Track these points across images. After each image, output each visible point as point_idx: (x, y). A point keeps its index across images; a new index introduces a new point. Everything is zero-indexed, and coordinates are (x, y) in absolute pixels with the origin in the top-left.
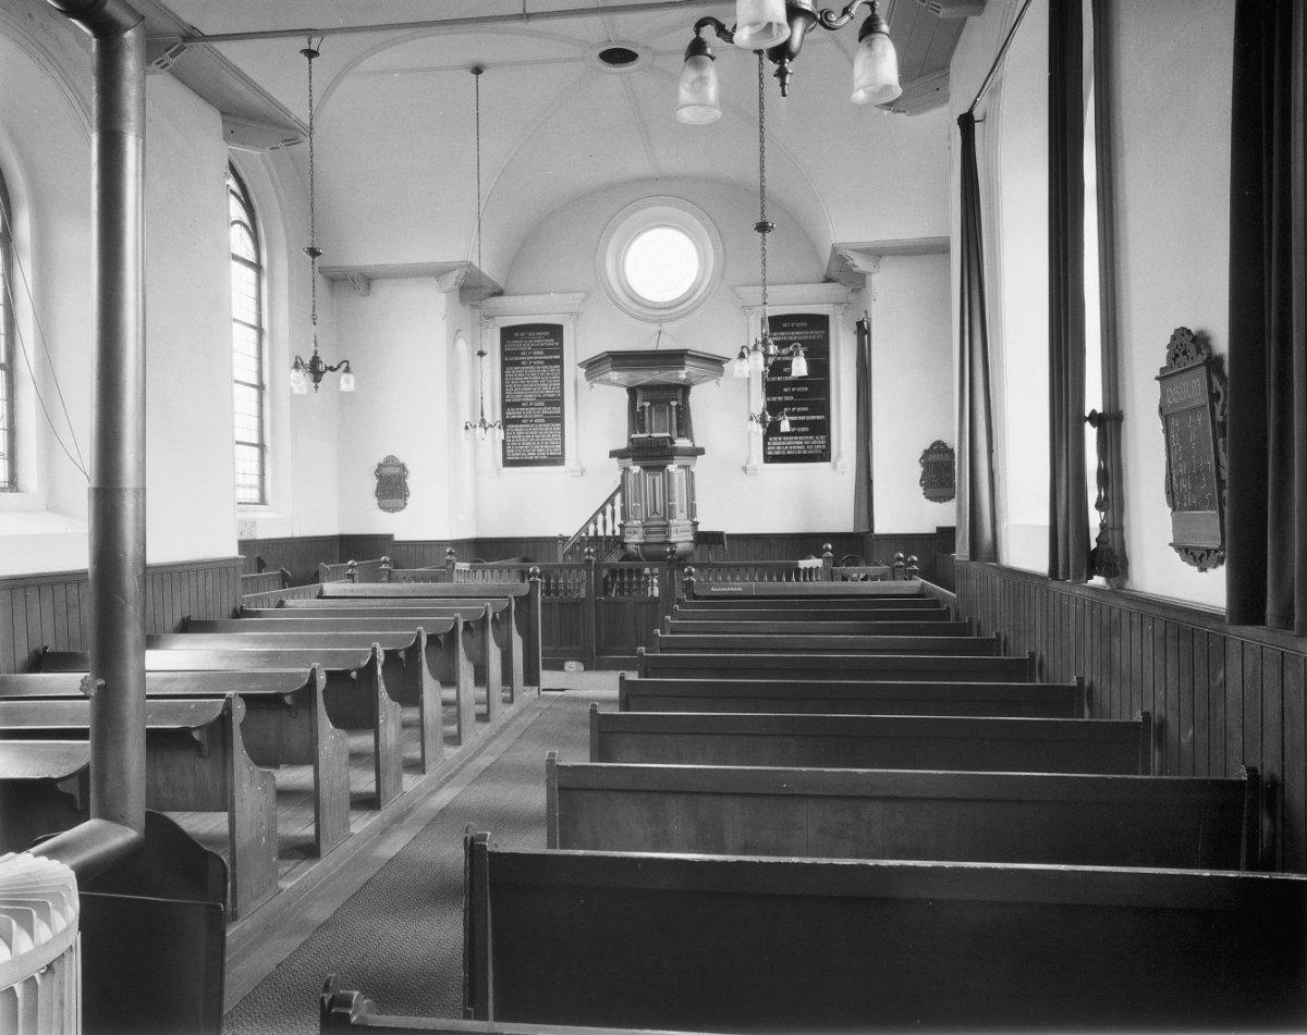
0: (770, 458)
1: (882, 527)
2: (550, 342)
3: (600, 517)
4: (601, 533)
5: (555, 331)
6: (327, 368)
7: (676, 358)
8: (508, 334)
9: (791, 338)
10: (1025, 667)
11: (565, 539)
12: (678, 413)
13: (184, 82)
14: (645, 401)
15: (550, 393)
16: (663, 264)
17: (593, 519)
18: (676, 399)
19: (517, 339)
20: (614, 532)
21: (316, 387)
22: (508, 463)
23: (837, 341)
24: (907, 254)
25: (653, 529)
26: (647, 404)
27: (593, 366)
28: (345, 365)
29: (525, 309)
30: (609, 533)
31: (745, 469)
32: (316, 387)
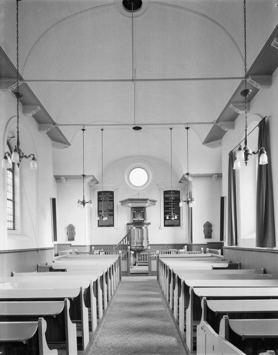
0: (165, 226)
1: (194, 243)
2: (111, 196)
3: (124, 240)
4: (124, 244)
5: (112, 193)
6: (86, 202)
7: (145, 200)
8: (99, 193)
9: (175, 195)
10: (110, 268)
11: (115, 245)
12: (143, 214)
13: (48, 135)
14: (135, 211)
15: (110, 208)
16: (139, 178)
17: (123, 240)
18: (142, 211)
19: (102, 195)
20: (128, 243)
21: (84, 207)
22: (99, 226)
23: (182, 196)
24: (207, 177)
25: (138, 243)
26: (135, 212)
27: (123, 202)
28: (90, 202)
29: (107, 187)
30: (126, 244)
31: (159, 228)
32: (84, 207)
